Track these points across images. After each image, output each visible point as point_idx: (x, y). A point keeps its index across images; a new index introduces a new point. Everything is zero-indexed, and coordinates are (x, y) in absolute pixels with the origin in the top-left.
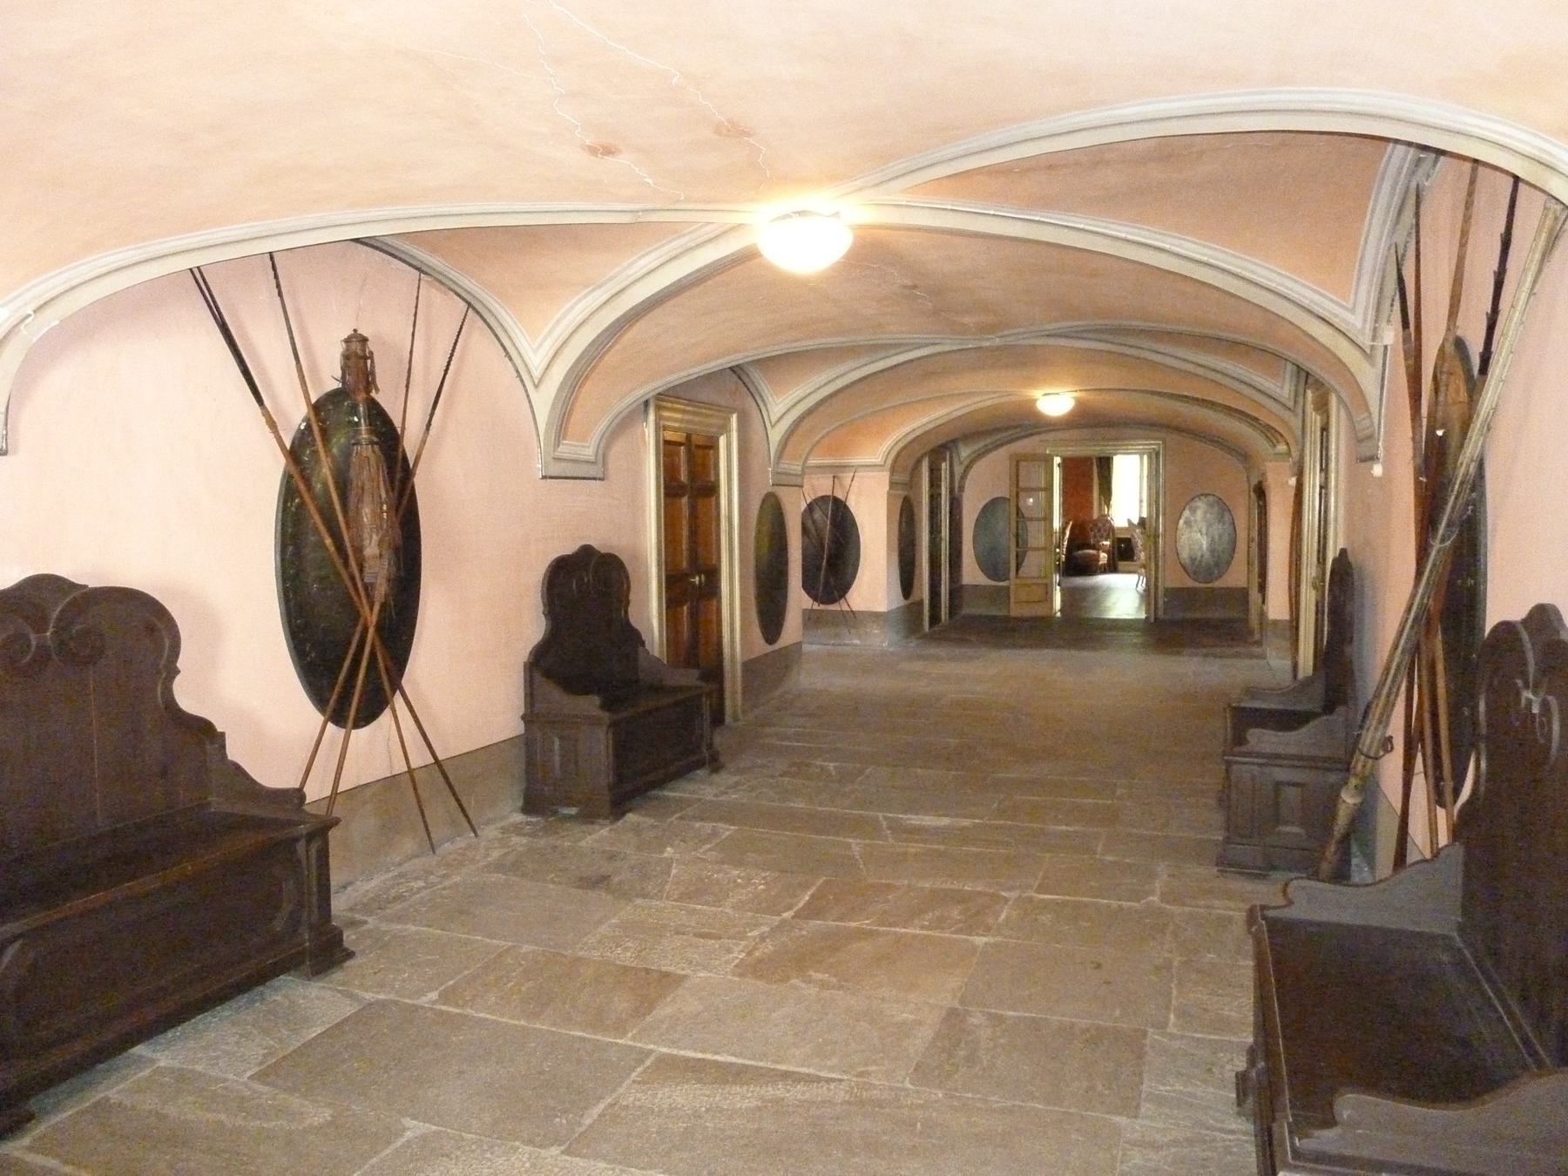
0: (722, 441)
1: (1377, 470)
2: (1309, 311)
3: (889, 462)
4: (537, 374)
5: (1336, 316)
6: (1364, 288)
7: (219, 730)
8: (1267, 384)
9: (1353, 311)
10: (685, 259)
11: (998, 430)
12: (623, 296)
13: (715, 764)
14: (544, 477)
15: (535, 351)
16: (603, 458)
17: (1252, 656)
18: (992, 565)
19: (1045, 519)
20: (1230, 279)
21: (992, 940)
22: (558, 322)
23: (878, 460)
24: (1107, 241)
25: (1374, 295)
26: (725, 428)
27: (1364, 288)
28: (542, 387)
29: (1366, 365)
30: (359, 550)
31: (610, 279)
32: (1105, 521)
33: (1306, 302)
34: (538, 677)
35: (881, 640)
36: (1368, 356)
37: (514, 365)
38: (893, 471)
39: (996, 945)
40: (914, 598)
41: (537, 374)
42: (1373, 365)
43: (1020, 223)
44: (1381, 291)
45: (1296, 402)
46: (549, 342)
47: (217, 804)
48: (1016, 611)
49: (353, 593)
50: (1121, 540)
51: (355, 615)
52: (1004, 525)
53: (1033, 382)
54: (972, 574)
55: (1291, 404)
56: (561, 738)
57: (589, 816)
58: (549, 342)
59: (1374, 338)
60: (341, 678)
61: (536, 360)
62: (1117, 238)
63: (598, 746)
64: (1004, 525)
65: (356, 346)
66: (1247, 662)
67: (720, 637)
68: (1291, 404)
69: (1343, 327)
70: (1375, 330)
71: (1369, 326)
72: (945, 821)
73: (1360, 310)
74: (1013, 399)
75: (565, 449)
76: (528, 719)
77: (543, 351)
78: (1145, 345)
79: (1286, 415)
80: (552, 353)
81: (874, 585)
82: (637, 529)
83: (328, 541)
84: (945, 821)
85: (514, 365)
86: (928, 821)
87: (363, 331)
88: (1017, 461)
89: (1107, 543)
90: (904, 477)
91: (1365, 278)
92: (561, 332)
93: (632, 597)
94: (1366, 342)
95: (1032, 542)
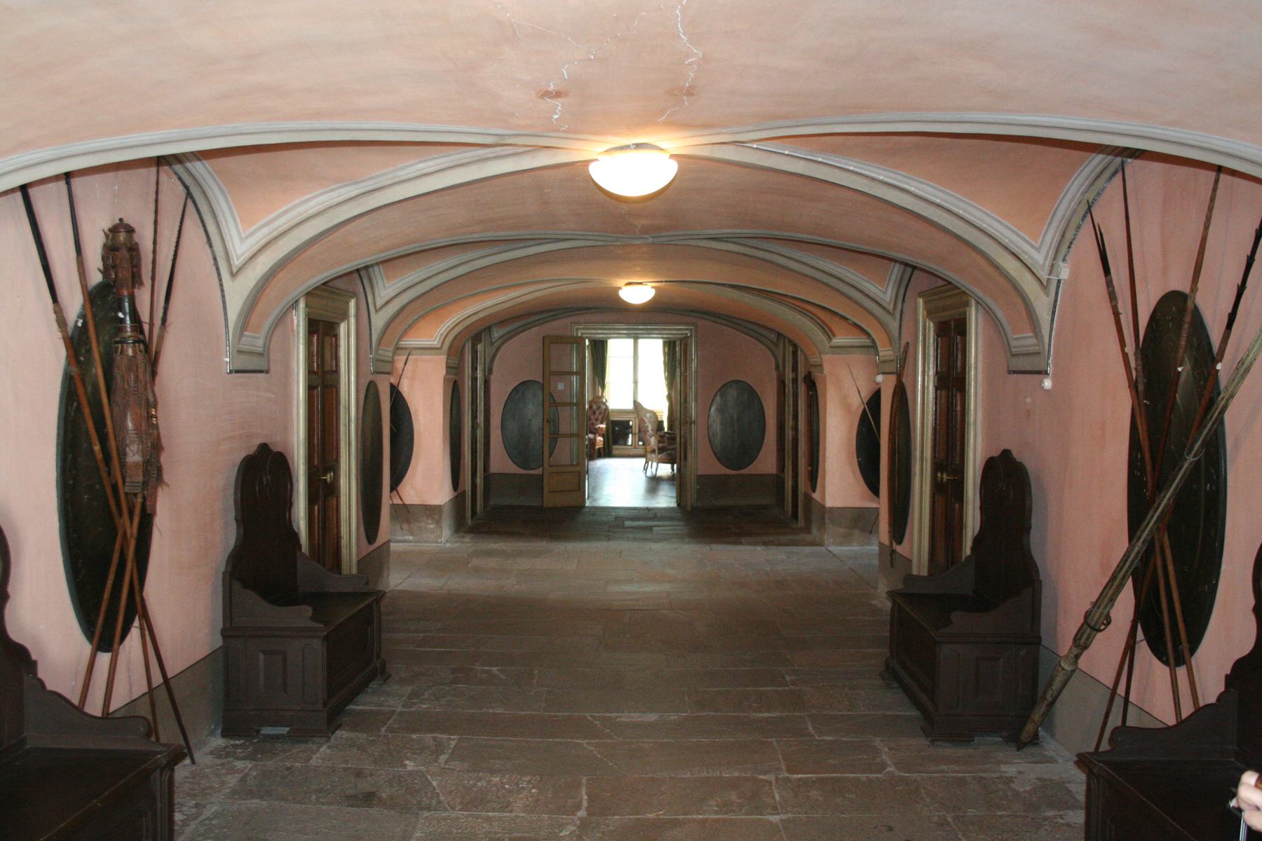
0: (343, 328)
1: (1048, 384)
2: (1006, 248)
3: (446, 347)
4: (237, 263)
5: (1026, 253)
6: (1051, 231)
7: (34, 657)
8: (873, 289)
9: (1038, 250)
10: (474, 167)
11: (536, 313)
12: (377, 195)
13: (382, 673)
14: (231, 372)
15: (242, 240)
16: (267, 346)
17: (812, 544)
18: (520, 450)
19: (577, 404)
20: (961, 223)
21: (784, 817)
22: (285, 212)
23: (435, 343)
24: (865, 181)
25: (1057, 238)
26: (344, 316)
27: (1051, 231)
28: (241, 278)
29: (1042, 295)
30: (122, 455)
31: (372, 178)
32: (598, 401)
33: (1006, 241)
34: (237, 585)
35: (442, 537)
36: (1045, 287)
37: (213, 253)
38: (449, 355)
39: (788, 820)
40: (460, 490)
41: (237, 263)
42: (1047, 295)
43: (802, 162)
44: (1063, 236)
45: (894, 309)
46: (265, 231)
47: (36, 738)
48: (549, 501)
49: (112, 502)
50: (615, 423)
51: (112, 530)
52: (532, 409)
53: (618, 273)
54: (501, 462)
55: (891, 308)
56: (264, 653)
57: (304, 732)
58: (265, 231)
59: (1050, 273)
60: (106, 595)
61: (240, 248)
62: (873, 179)
63: (308, 654)
64: (532, 409)
65: (122, 237)
66: (807, 549)
67: (339, 538)
68: (891, 308)
69: (1029, 262)
70: (1052, 266)
71: (1048, 263)
72: (652, 717)
73: (1044, 249)
74: (589, 285)
75: (246, 344)
76: (225, 633)
77: (252, 240)
78: (403, 174)
79: (886, 318)
80: (262, 243)
81: (428, 479)
82: (286, 427)
83: (97, 448)
84: (652, 717)
85: (213, 253)
86: (636, 717)
87: (129, 220)
88: (550, 341)
89: (603, 426)
90: (454, 362)
91: (1055, 224)
92: (282, 223)
93: (1033, 521)
94: (1044, 275)
95: (563, 429)
